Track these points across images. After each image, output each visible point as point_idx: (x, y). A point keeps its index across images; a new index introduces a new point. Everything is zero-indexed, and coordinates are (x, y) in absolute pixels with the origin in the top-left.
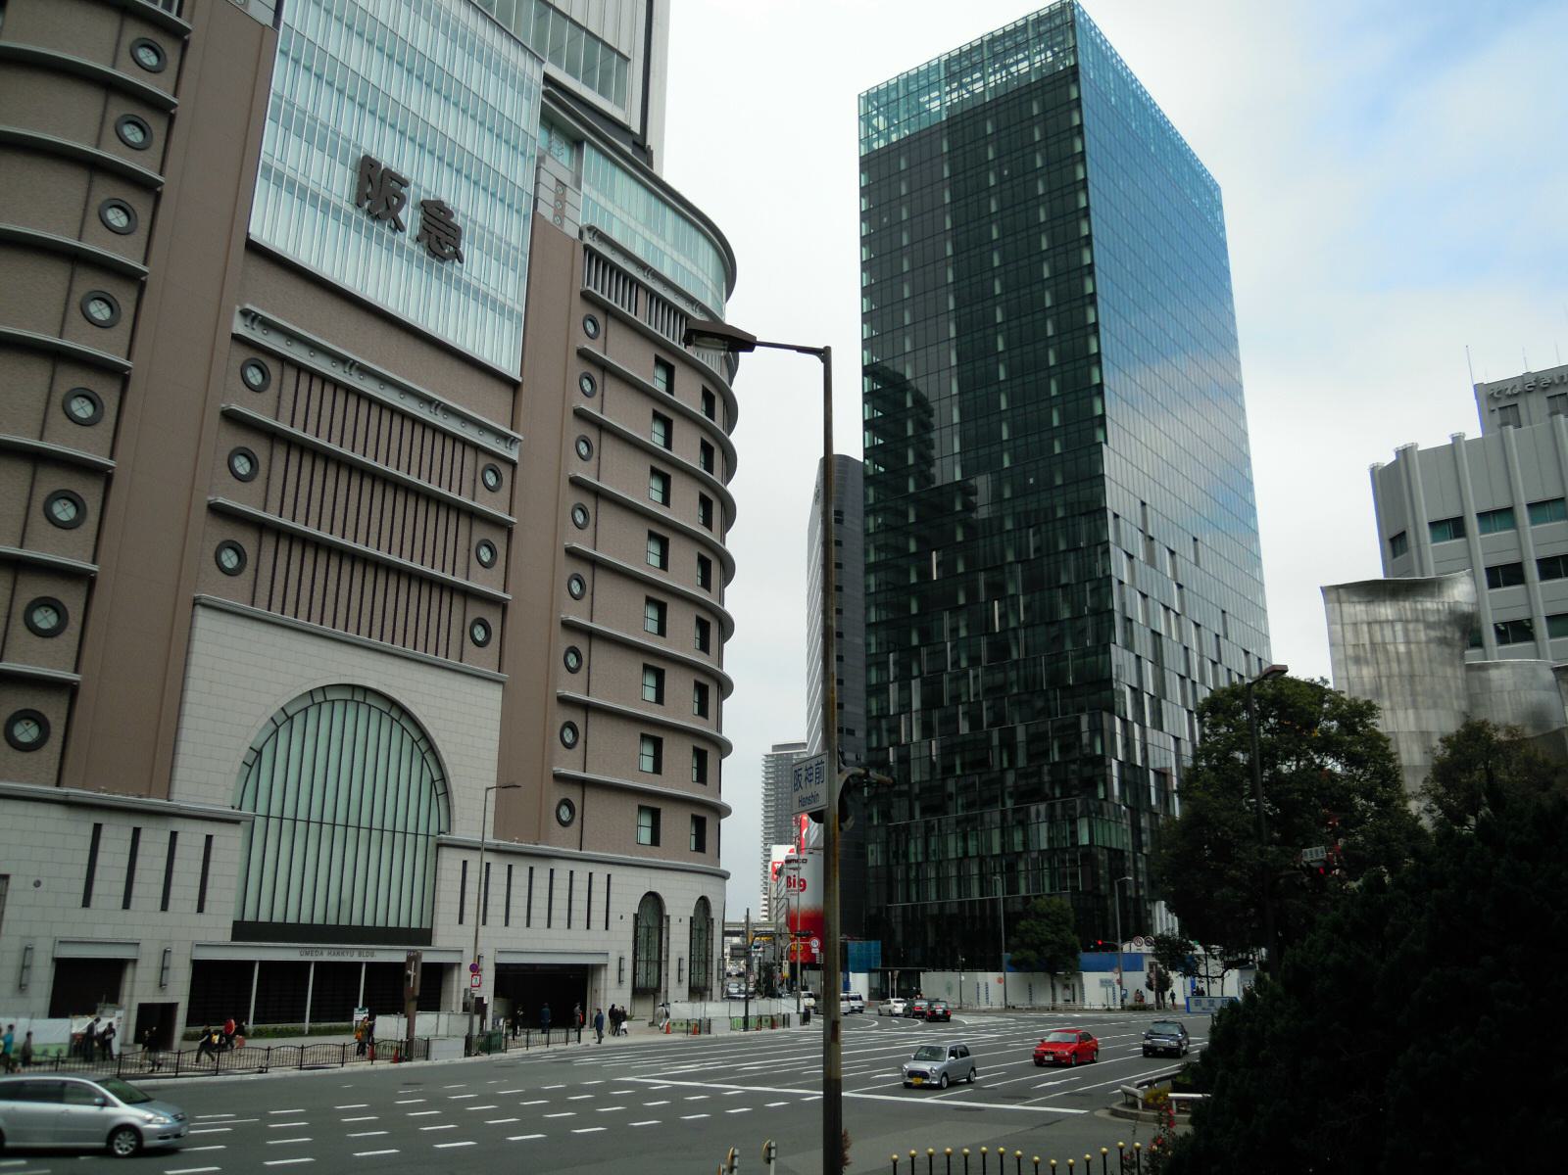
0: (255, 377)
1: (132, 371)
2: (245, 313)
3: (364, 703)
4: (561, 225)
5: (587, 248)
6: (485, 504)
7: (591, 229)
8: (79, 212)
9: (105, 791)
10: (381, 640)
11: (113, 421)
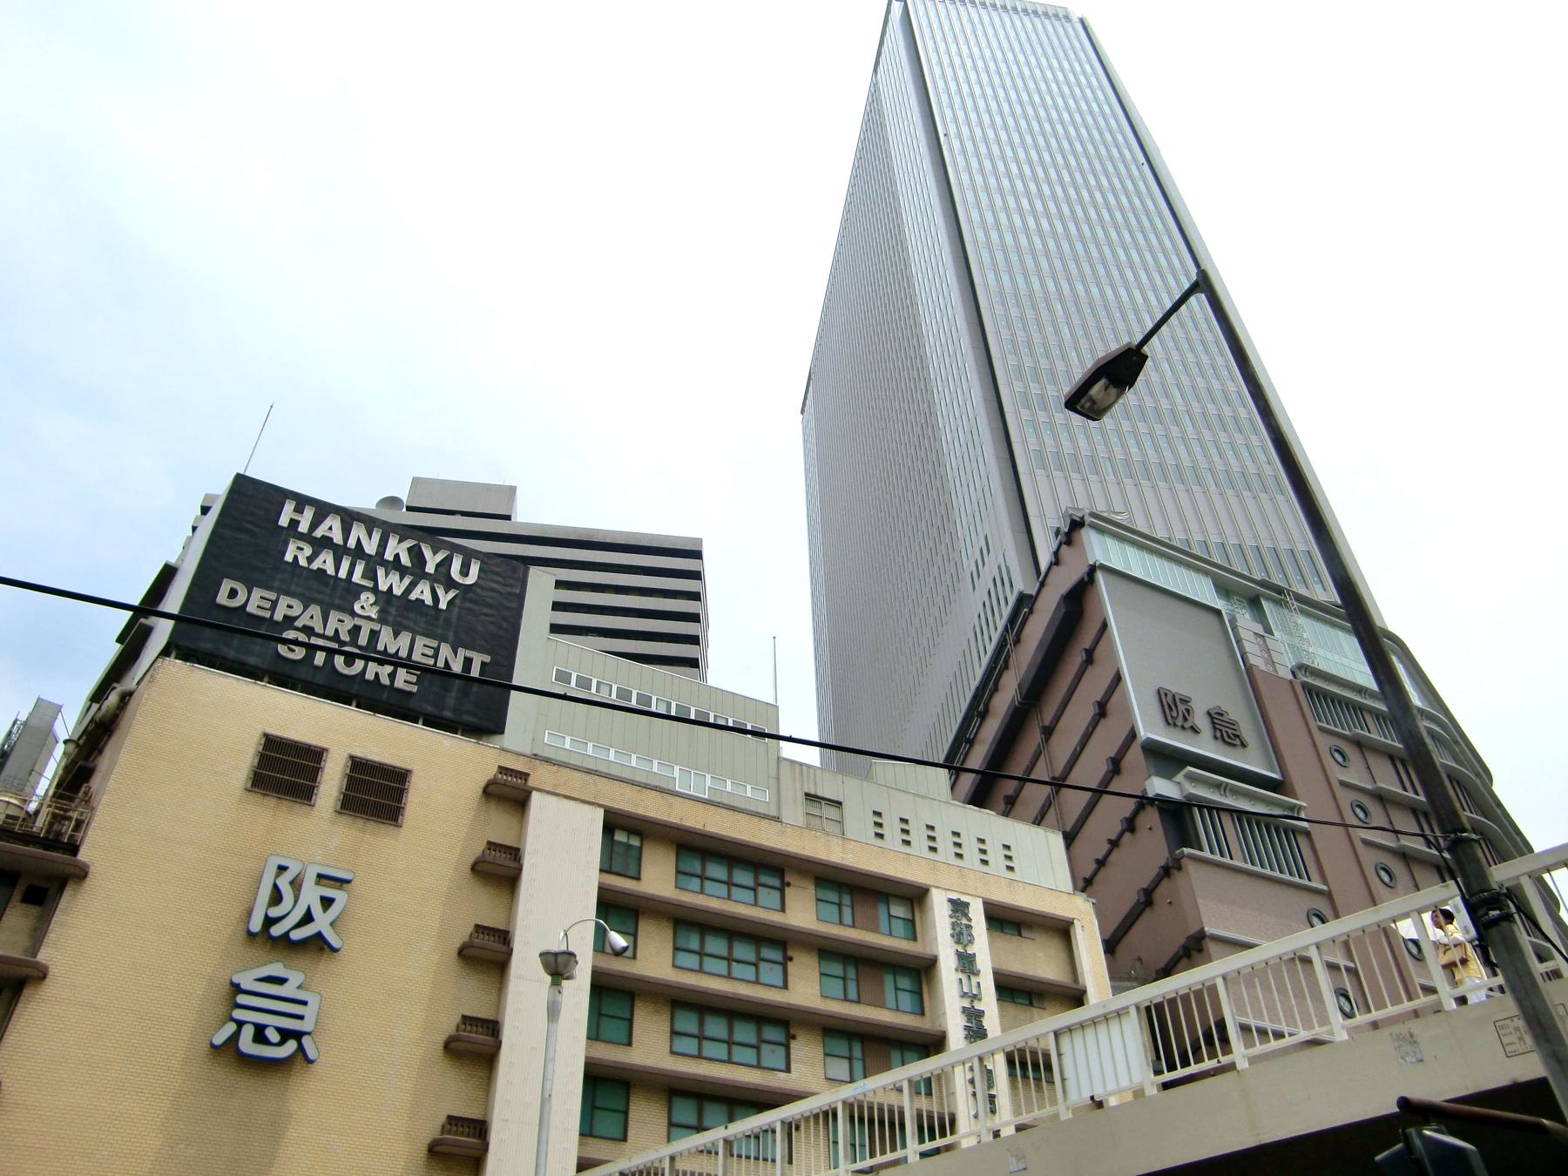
5: (1305, 686)
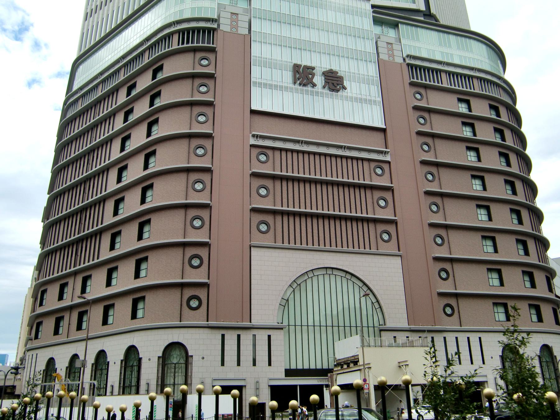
0: (379, 171)
1: (394, 187)
2: (253, 136)
3: (332, 274)
4: (394, 59)
5: (408, 65)
6: (377, 182)
7: (408, 56)
8: (189, 121)
9: (223, 322)
10: (378, 250)
11: (210, 188)
